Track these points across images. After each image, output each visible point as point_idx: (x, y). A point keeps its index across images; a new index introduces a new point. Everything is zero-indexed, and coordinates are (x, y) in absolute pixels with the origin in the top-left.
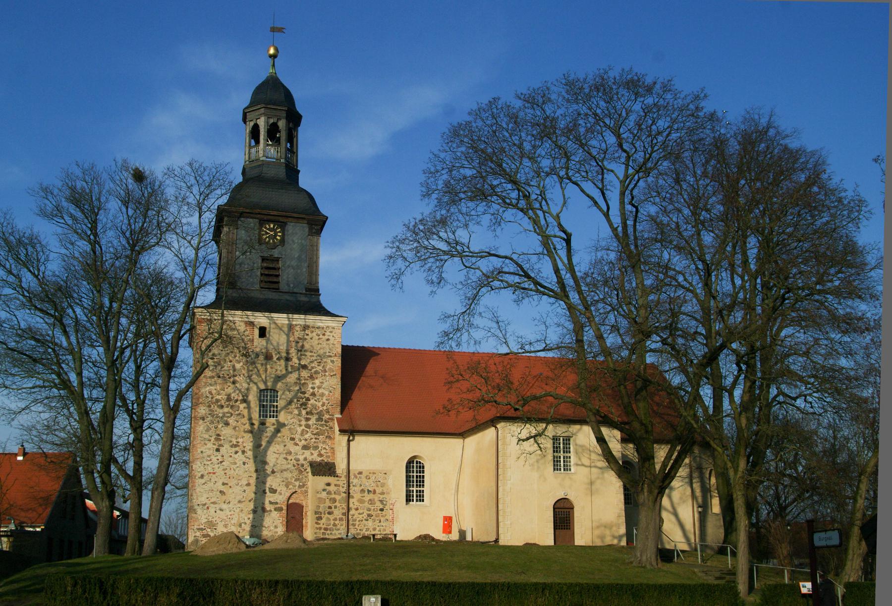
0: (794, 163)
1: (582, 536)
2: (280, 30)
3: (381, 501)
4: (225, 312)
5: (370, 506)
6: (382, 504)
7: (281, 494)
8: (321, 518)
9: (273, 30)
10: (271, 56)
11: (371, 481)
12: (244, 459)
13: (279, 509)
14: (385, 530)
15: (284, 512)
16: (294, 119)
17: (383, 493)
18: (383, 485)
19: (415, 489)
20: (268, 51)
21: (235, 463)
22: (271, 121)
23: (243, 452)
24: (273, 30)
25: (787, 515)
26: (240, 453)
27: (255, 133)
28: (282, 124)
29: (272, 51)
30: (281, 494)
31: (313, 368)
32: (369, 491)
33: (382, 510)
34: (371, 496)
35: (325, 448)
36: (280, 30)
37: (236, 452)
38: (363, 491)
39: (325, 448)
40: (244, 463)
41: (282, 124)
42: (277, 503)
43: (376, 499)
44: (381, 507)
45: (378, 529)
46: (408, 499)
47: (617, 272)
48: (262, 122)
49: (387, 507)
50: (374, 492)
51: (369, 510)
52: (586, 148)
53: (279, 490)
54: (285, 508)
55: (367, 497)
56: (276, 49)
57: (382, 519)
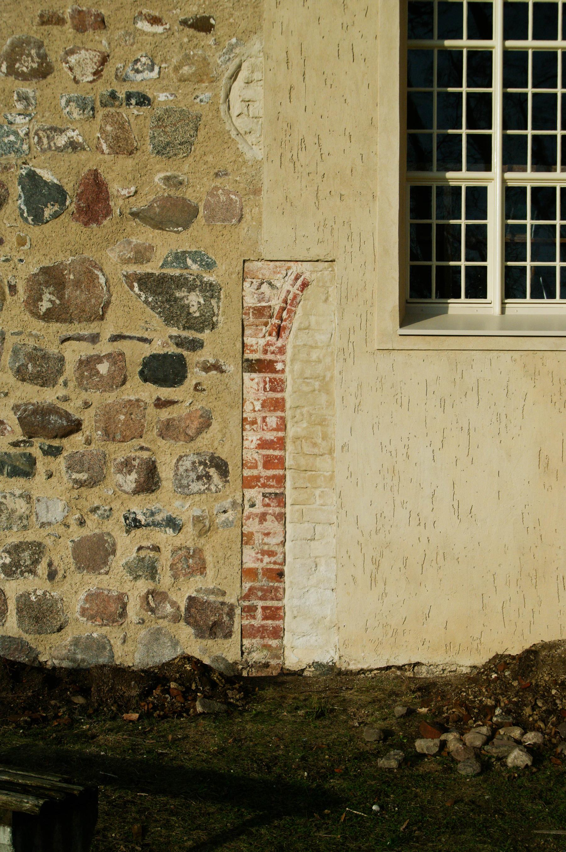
0: (141, 252)
3: (161, 289)
5: (48, 335)
6: (174, 313)
11: (58, 90)
14: (192, 562)
17: (175, 214)
18: (179, 135)
19: (494, 181)
25: (463, 714)
33: (165, 370)
43: (113, 263)
44: (162, 339)
45: (127, 547)
46: (433, 271)
47: (168, 149)
49: (215, 345)
50: (94, 201)
51: (40, 368)
57: (169, 458)
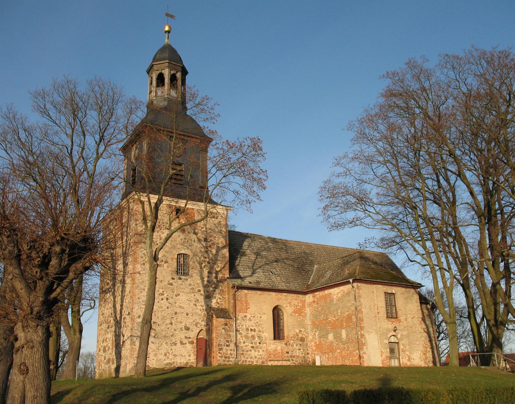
1: (122, 375)
2: (172, 17)
4: (164, 198)
7: (192, 331)
8: (222, 349)
9: (167, 15)
10: (166, 32)
12: (168, 305)
13: (192, 343)
15: (195, 344)
16: (184, 72)
20: (165, 28)
21: (162, 307)
22: (173, 72)
23: (167, 299)
24: (167, 15)
26: (165, 300)
27: (161, 79)
28: (179, 75)
29: (167, 28)
30: (192, 331)
31: (211, 240)
32: (251, 330)
34: (253, 333)
35: (220, 298)
36: (172, 17)
37: (162, 299)
38: (247, 329)
39: (220, 298)
40: (168, 308)
41: (179, 75)
42: (190, 338)
48: (167, 73)
50: (255, 331)
52: (102, 148)
53: (191, 327)
54: (195, 341)
55: (250, 334)
56: (170, 27)
